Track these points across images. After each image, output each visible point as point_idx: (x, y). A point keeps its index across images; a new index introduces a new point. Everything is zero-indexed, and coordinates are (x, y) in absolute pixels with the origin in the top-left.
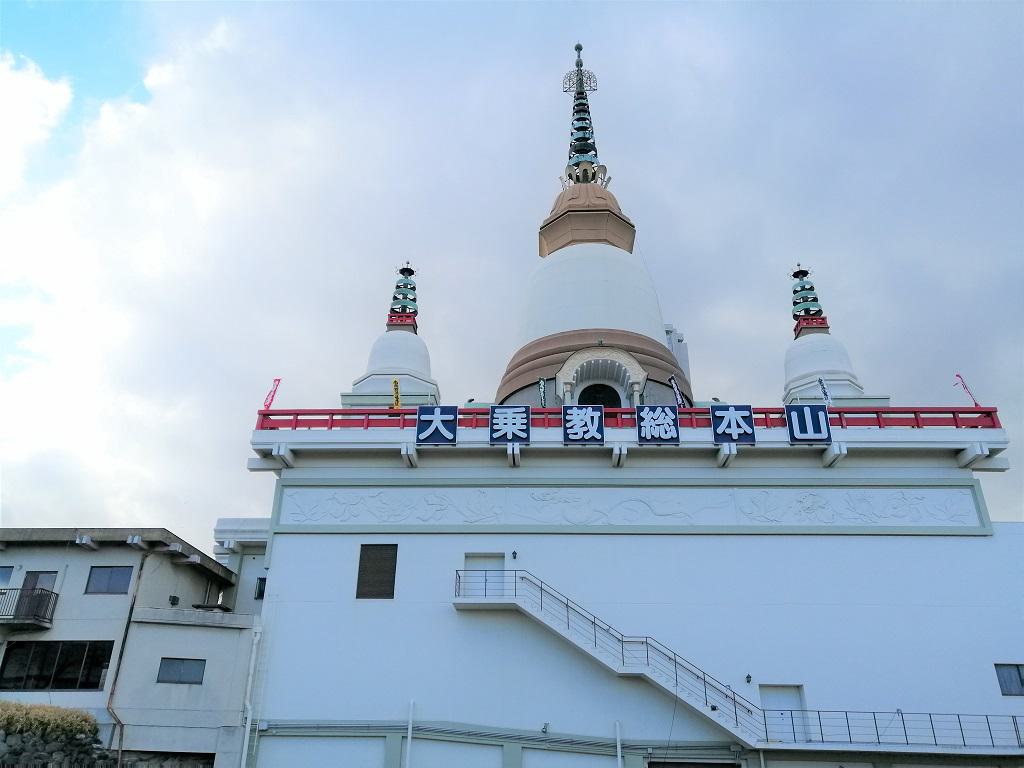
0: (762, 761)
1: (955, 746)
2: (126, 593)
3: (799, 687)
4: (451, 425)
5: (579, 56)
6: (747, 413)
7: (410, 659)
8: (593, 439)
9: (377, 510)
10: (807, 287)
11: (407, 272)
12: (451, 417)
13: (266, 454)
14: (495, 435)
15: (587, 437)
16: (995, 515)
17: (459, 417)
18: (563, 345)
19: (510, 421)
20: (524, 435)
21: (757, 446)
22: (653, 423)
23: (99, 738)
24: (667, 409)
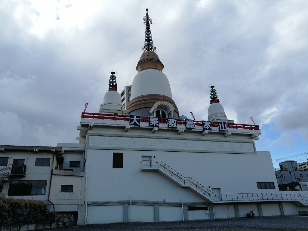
1: (252, 200)
2: (79, 167)
3: (219, 189)
4: (138, 121)
5: (147, 12)
6: (210, 123)
7: (129, 184)
8: (175, 127)
9: (119, 143)
11: (212, 87)
12: (139, 119)
14: (151, 125)
15: (174, 126)
16: (258, 149)
18: (151, 98)
20: (158, 125)
21: (212, 131)
22: (189, 124)
23: (47, 208)
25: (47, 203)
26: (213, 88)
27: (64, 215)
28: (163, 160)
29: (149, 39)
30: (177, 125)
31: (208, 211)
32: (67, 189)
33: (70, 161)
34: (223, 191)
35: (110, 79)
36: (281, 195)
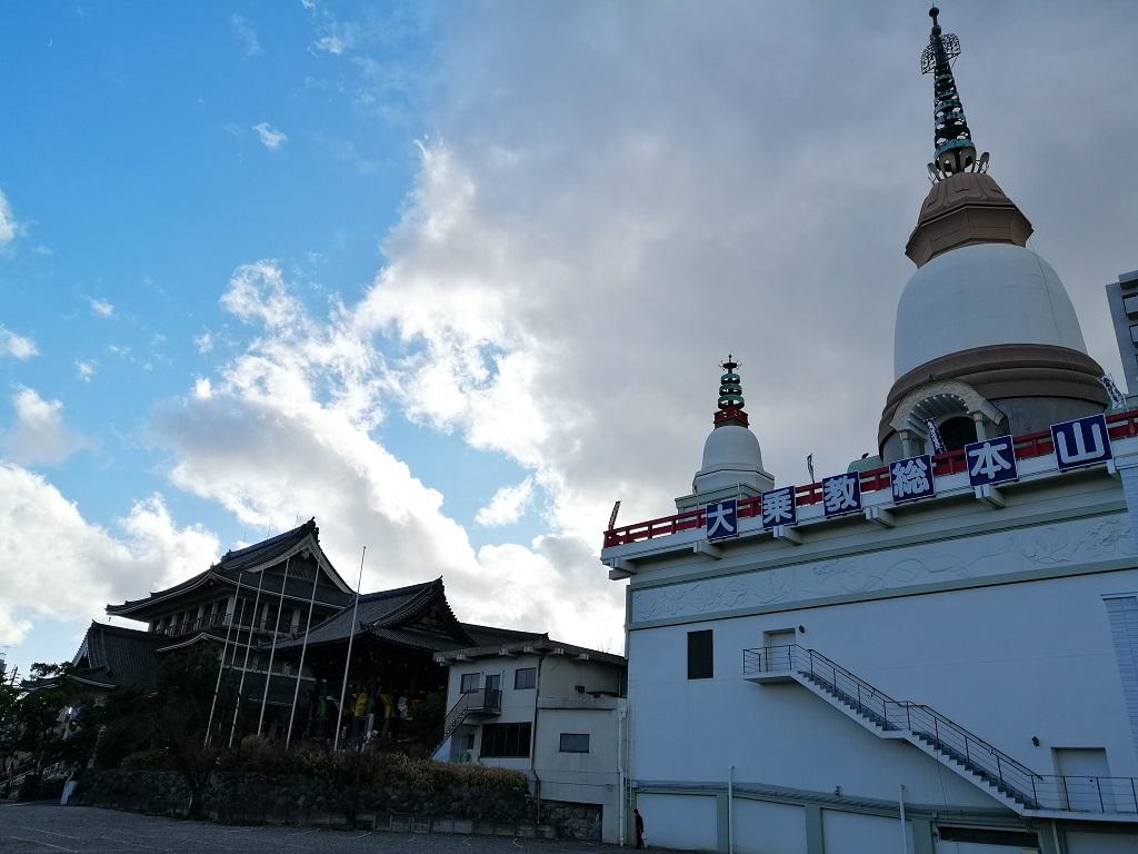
5: (935, 23)
6: (1004, 446)
8: (850, 508)
11: (730, 366)
12: (730, 511)
14: (767, 521)
15: (844, 506)
17: (738, 508)
18: (983, 362)
19: (777, 505)
20: (789, 516)
22: (905, 479)
28: (833, 641)
29: (951, 127)
30: (856, 497)
32: (574, 743)
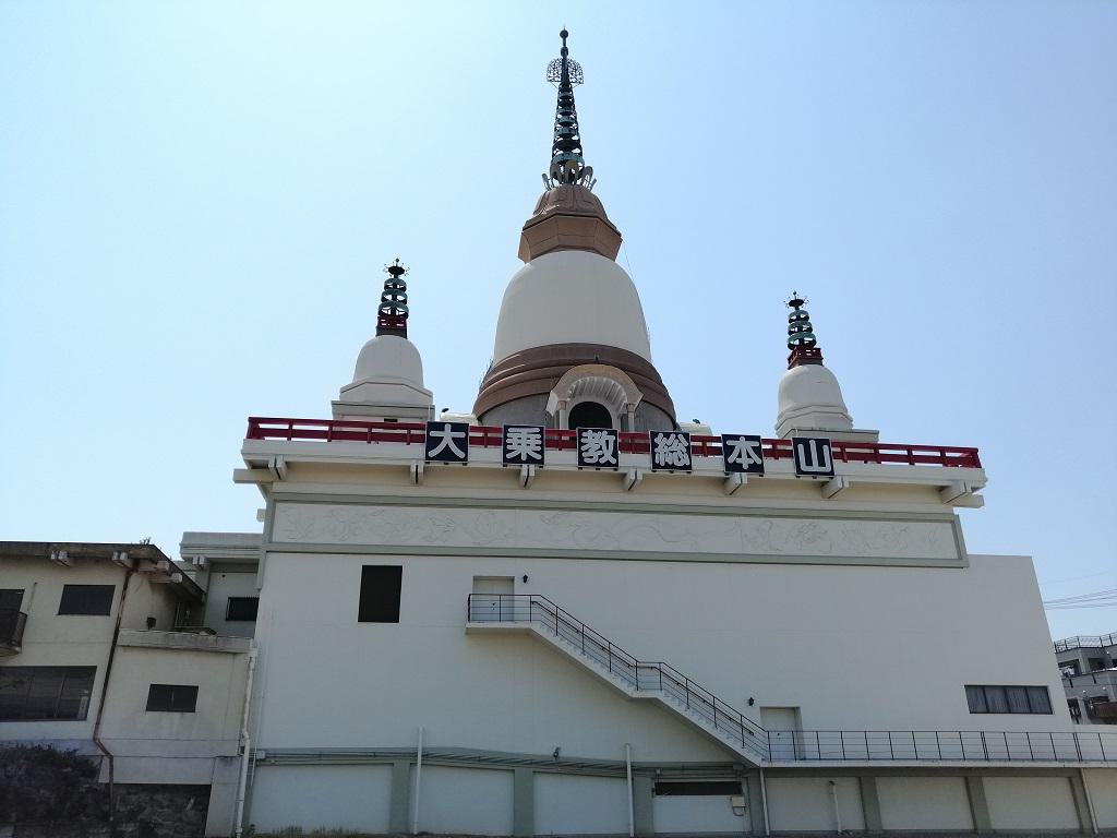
0: (762, 779)
1: (933, 760)
3: (795, 710)
5: (565, 44)
6: (756, 444)
7: (424, 682)
8: (608, 464)
10: (802, 316)
12: (462, 435)
13: (254, 466)
14: (509, 456)
15: (602, 461)
16: (972, 548)
17: (471, 434)
20: (539, 457)
22: (667, 450)
24: (680, 436)
25: (88, 750)
26: (797, 308)
27: (159, 797)
29: (567, 141)
30: (615, 455)
31: (739, 801)
32: (172, 698)
33: (230, 598)
34: (808, 720)
35: (792, 327)
36: (1076, 738)
